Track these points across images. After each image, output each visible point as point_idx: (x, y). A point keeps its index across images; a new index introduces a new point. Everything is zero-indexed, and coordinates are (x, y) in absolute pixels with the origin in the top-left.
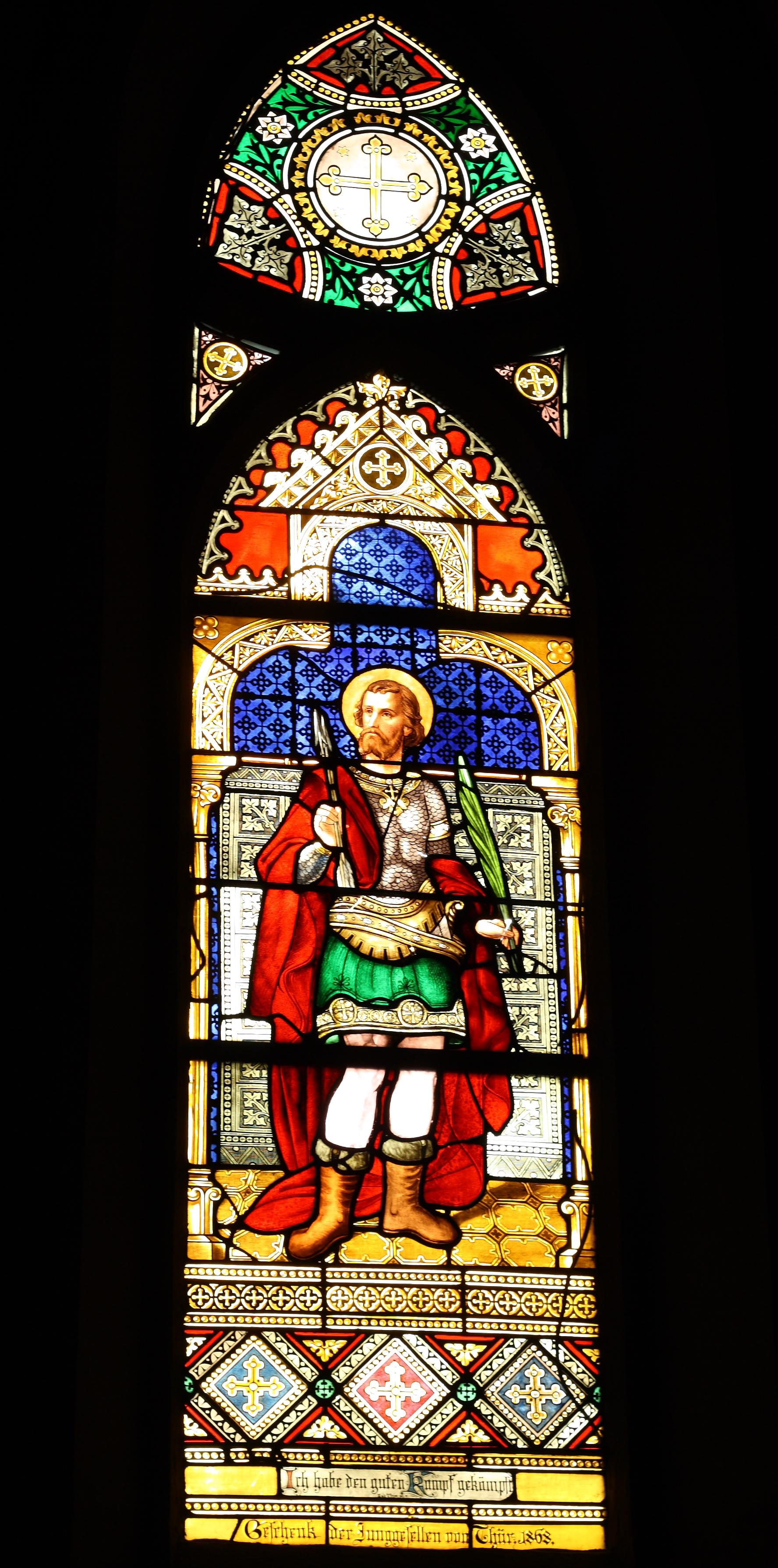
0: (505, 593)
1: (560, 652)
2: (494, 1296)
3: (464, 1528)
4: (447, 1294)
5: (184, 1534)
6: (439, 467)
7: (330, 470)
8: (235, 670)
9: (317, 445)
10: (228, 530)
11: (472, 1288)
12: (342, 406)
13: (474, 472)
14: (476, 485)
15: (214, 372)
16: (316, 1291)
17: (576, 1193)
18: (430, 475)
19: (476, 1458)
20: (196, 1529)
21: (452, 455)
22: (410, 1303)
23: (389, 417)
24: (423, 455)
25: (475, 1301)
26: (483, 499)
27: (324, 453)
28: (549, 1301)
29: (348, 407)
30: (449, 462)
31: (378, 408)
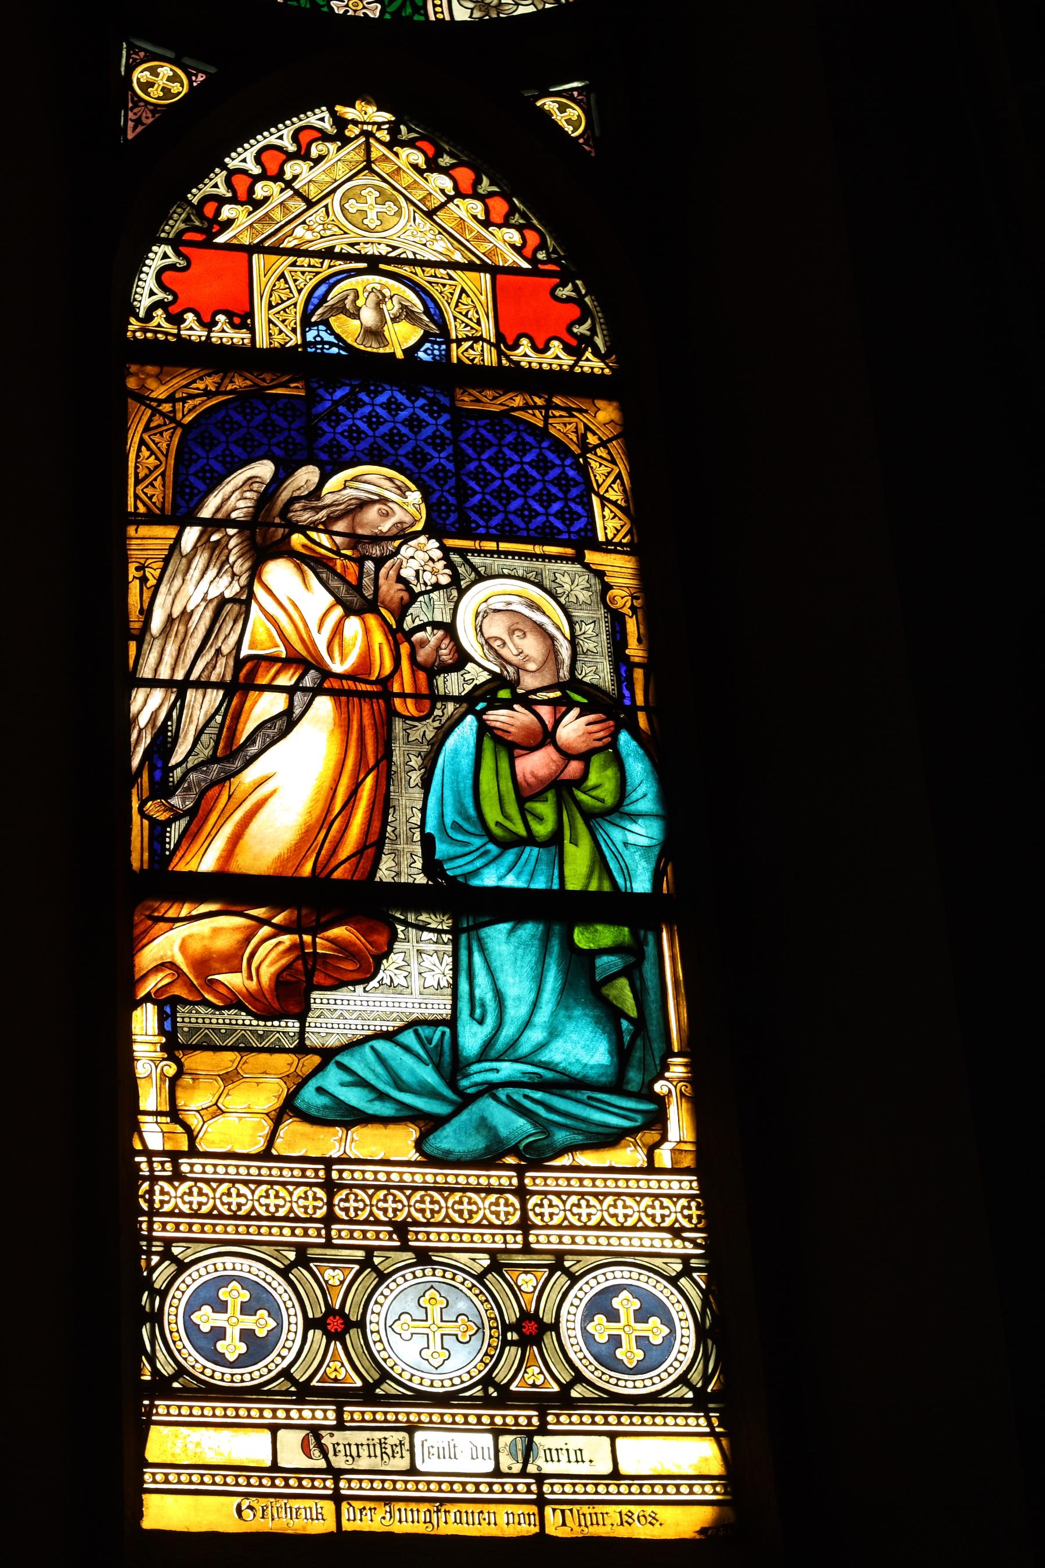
0: (534, 348)
1: (606, 414)
2: (253, 1192)
3: (329, 1506)
4: (657, 1203)
5: (141, 1515)
6: (442, 206)
7: (303, 206)
8: (179, 424)
9: (288, 176)
10: (172, 267)
11: (533, 1193)
12: (317, 135)
13: (487, 211)
14: (491, 229)
15: (148, 95)
16: (512, 1199)
17: (672, 1068)
18: (430, 214)
19: (157, 1407)
20: (163, 1513)
21: (459, 194)
22: (643, 1215)
23: (378, 150)
24: (422, 194)
25: (538, 1210)
26: (504, 244)
27: (297, 185)
28: (179, 1193)
29: (325, 137)
30: (456, 201)
31: (363, 139)
